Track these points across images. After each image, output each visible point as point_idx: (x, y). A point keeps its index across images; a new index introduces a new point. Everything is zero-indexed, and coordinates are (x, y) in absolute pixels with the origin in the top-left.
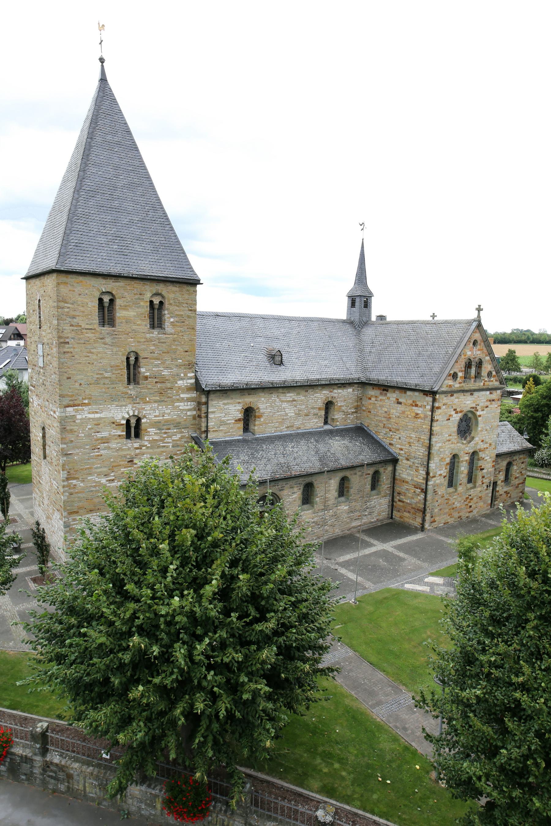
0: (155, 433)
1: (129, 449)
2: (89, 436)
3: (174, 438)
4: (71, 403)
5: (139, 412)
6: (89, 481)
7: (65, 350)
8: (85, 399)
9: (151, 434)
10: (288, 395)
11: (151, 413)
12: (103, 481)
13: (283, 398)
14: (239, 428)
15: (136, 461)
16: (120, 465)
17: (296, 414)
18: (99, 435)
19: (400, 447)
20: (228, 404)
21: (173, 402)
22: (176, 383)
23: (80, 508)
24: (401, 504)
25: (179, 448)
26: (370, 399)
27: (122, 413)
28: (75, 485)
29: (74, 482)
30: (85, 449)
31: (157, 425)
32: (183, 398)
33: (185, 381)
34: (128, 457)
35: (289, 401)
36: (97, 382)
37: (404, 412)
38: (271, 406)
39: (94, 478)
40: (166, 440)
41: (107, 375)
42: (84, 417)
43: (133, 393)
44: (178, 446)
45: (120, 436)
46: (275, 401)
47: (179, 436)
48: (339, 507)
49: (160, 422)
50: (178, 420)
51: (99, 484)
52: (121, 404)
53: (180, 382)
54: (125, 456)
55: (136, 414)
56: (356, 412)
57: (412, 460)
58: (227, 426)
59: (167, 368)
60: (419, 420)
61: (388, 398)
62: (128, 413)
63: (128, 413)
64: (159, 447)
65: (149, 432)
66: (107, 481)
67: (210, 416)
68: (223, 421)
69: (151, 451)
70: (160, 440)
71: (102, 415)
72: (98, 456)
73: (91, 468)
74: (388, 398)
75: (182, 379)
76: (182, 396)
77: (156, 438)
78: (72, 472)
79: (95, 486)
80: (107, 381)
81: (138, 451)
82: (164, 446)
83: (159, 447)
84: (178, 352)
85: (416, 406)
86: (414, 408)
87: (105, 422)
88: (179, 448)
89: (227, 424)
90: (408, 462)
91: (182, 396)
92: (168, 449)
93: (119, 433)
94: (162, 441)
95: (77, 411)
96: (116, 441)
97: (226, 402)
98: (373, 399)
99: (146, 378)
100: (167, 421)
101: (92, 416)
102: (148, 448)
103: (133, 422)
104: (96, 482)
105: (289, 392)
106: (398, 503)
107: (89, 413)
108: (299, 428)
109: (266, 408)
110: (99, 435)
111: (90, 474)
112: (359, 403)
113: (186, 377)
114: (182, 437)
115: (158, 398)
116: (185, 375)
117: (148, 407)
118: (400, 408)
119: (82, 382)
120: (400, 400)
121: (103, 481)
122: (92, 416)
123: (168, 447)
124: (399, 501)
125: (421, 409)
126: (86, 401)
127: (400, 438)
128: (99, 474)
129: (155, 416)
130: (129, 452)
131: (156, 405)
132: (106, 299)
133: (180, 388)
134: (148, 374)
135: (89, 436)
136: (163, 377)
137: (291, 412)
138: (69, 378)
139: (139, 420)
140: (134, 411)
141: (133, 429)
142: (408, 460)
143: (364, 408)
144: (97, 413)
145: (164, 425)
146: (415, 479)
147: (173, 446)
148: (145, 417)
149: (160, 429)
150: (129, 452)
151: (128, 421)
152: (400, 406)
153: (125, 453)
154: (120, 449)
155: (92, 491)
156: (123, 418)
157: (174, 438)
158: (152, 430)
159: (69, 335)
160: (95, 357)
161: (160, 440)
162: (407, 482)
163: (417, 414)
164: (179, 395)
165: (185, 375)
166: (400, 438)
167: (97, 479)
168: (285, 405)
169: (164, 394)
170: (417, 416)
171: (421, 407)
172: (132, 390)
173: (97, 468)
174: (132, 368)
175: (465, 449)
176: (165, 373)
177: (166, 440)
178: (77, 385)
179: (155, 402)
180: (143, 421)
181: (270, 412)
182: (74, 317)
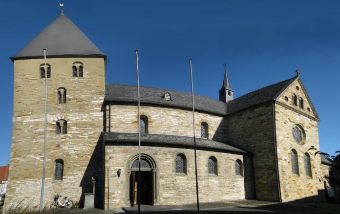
0: (76, 130)
1: (57, 139)
2: (31, 131)
3: (90, 133)
4: (20, 114)
5: (65, 117)
6: (28, 158)
7: (18, 90)
8: (29, 112)
9: (73, 130)
10: (173, 112)
11: (73, 118)
12: (38, 158)
13: (169, 113)
14: (136, 127)
15: (61, 146)
16: (50, 149)
17: (179, 125)
18: (37, 131)
19: (253, 145)
20: (126, 111)
21: (89, 112)
22: (91, 102)
23: (20, 175)
24: (260, 185)
25: (93, 139)
26: (232, 124)
27: (53, 119)
28: (18, 161)
29: (18, 158)
30: (27, 138)
31: (77, 124)
32: (96, 110)
33: (97, 101)
34: (56, 143)
35: (174, 116)
36: (38, 103)
37: (253, 123)
38: (160, 117)
39: (32, 156)
40: (84, 134)
41: (43, 99)
42: (28, 121)
43: (61, 107)
44: (92, 138)
45: (51, 131)
46: (163, 114)
47: (93, 132)
48: (210, 180)
49: (79, 123)
50: (93, 122)
51: (35, 160)
52: (52, 113)
53: (94, 102)
54: (54, 143)
55: (63, 118)
56: (224, 133)
57: (263, 151)
58: (126, 125)
59: (84, 94)
60: (264, 123)
61: (243, 119)
62: (57, 118)
63: (57, 118)
64: (78, 138)
65: (71, 129)
66: (40, 158)
67: (112, 117)
68: (123, 122)
69: (73, 140)
70: (80, 134)
71: (39, 120)
72: (36, 143)
73: (30, 150)
74: (243, 119)
75: (96, 100)
76: (95, 109)
77: (76, 132)
78: (17, 152)
79: (32, 161)
80: (44, 102)
81: (63, 140)
82: (82, 138)
83: (78, 138)
84: (92, 87)
85: (262, 115)
86: (260, 117)
87: (41, 123)
88: (93, 139)
89: (126, 123)
90: (261, 154)
91: (95, 109)
92: (85, 140)
93: (51, 129)
94: (81, 134)
95: (24, 119)
96: (49, 134)
97: (124, 110)
98: (234, 123)
99: (70, 100)
100: (84, 122)
101: (33, 120)
102: (70, 138)
103: (62, 123)
104: (33, 159)
105: (173, 111)
106: (258, 186)
107: (32, 119)
108: (182, 134)
109: (156, 117)
110: (37, 131)
111: (29, 154)
112: (226, 129)
113: (98, 99)
114: (95, 133)
115: (78, 110)
116: (97, 98)
117: (71, 115)
118: (251, 121)
119: (28, 104)
120: (250, 117)
121: (38, 158)
122: (33, 120)
123: (85, 138)
124: (259, 184)
125: (265, 116)
126: (30, 113)
127: (253, 140)
128: (35, 154)
129: (76, 120)
130: (56, 141)
131: (77, 113)
132: (62, 91)
133: (93, 104)
134: (71, 98)
135: (31, 131)
136: (82, 99)
137: (176, 123)
138: (20, 102)
139: (65, 123)
140: (61, 117)
141: (62, 127)
142: (260, 152)
143: (229, 131)
144: (36, 118)
145: (82, 125)
146: (267, 164)
147: (89, 138)
148: (69, 120)
149: (80, 127)
150: (56, 141)
151: (58, 124)
152: (250, 120)
153: (53, 141)
154: (51, 139)
155: (29, 164)
156: (54, 121)
157: (90, 133)
158: (74, 128)
159: (21, 83)
160: (37, 91)
161: (80, 134)
162: (262, 168)
163: (262, 120)
164: (93, 108)
165: (97, 98)
166: (253, 140)
167: (34, 157)
168: (170, 118)
169: (82, 107)
170: (263, 121)
171: (265, 115)
172: (61, 106)
173: (34, 150)
174: (62, 96)
175: (301, 150)
176: (83, 97)
177: (84, 134)
178: (25, 106)
179: (76, 112)
180: (68, 122)
181: (159, 120)
182: (24, 75)
